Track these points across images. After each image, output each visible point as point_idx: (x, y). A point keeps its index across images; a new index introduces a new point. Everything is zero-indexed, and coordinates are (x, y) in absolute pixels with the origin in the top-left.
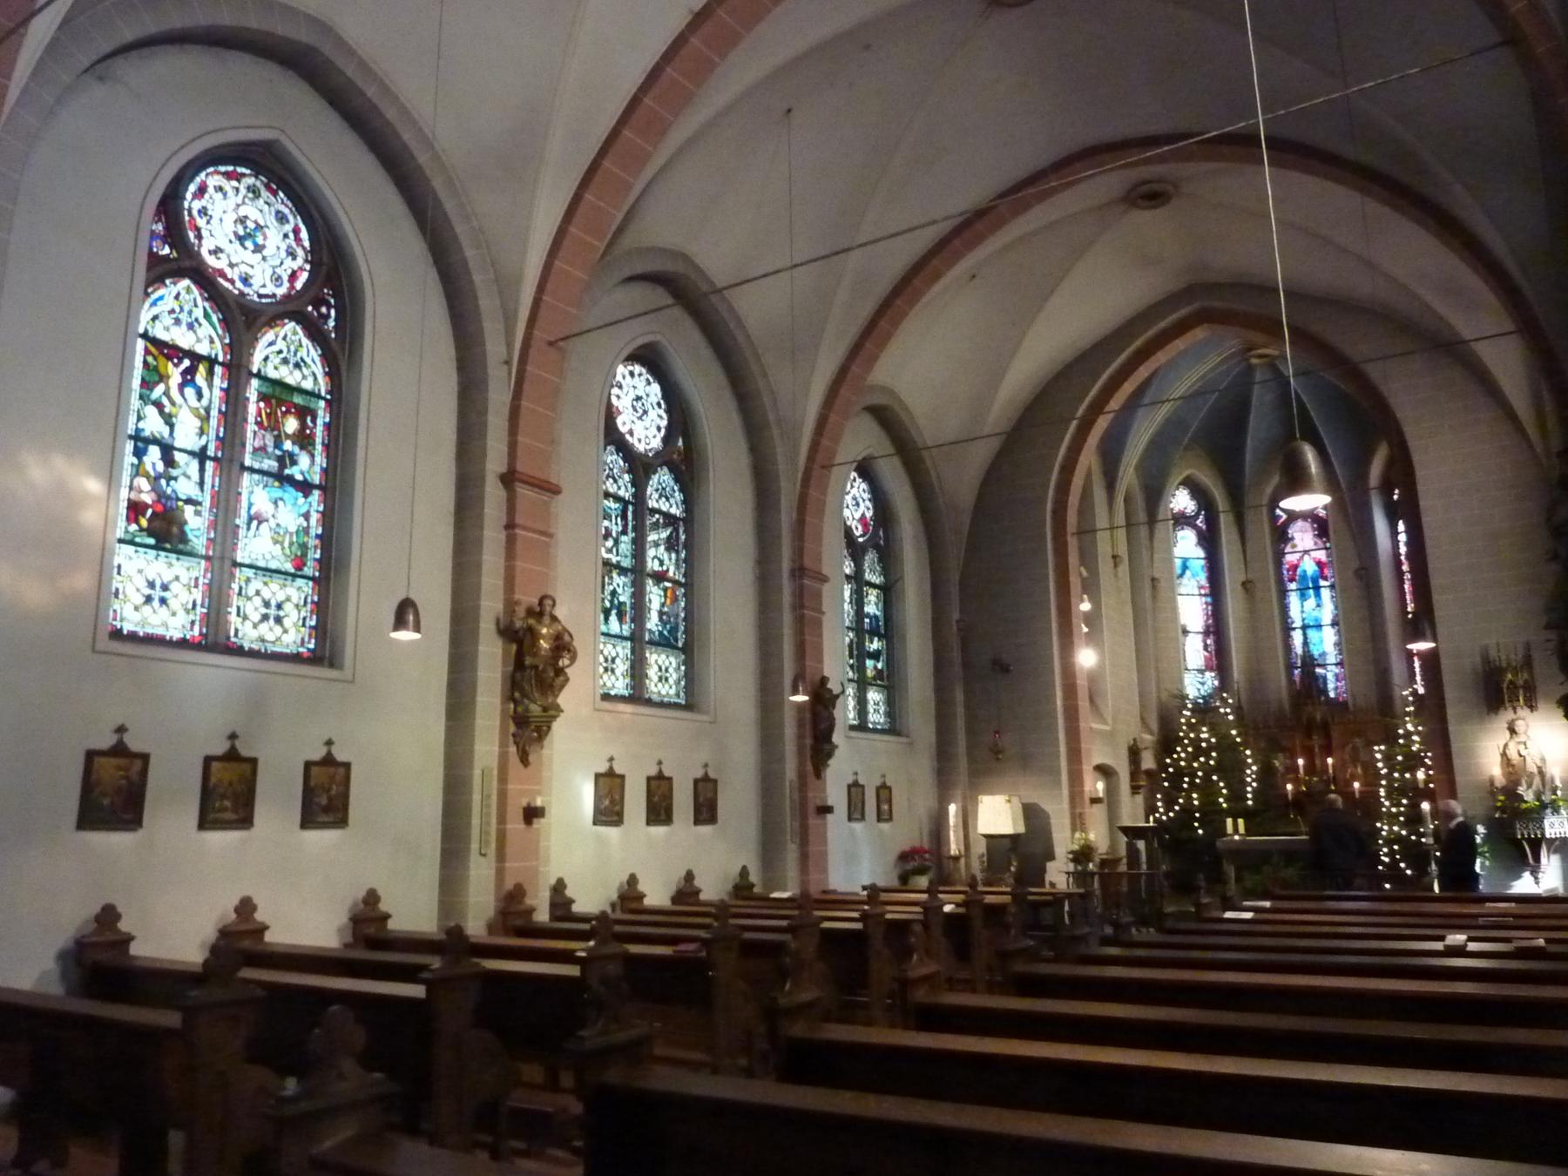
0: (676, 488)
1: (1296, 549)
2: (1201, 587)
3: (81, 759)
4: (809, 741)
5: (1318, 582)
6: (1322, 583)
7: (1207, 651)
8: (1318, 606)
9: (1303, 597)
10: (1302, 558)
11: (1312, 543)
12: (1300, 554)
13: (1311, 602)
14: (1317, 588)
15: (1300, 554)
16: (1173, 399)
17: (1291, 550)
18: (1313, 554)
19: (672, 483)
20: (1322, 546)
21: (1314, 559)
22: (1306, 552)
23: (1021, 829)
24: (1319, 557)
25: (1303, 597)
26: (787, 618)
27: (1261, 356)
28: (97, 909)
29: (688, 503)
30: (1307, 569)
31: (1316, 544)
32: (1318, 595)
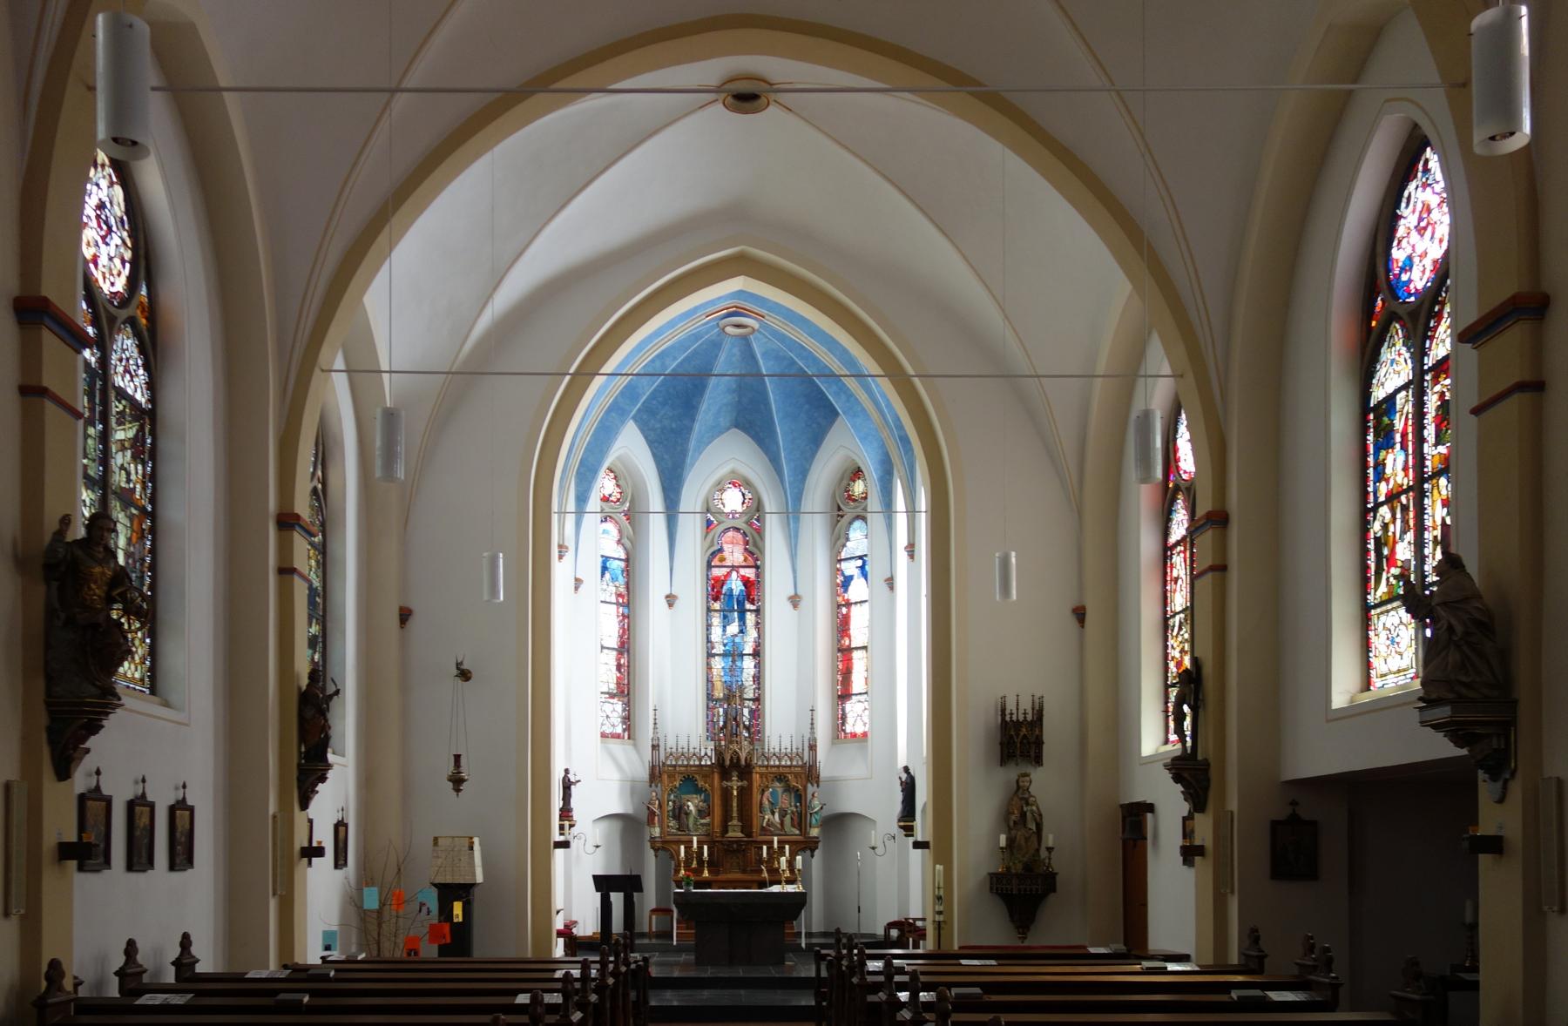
0: (140, 362)
1: (724, 564)
2: (619, 595)
3: (1181, 820)
4: (44, 720)
5: (744, 605)
6: (748, 606)
7: (620, 672)
8: (741, 631)
9: (726, 621)
10: (729, 574)
11: (742, 558)
12: (728, 570)
13: (733, 628)
14: (742, 613)
15: (728, 570)
16: (629, 375)
17: (718, 564)
18: (743, 572)
19: (136, 354)
20: (752, 563)
21: (743, 577)
22: (733, 568)
23: (813, 991)
24: (748, 575)
25: (726, 621)
26: (446, 384)
27: (738, 326)
28: (1473, 416)
29: (151, 386)
30: (733, 587)
31: (745, 560)
32: (742, 619)
